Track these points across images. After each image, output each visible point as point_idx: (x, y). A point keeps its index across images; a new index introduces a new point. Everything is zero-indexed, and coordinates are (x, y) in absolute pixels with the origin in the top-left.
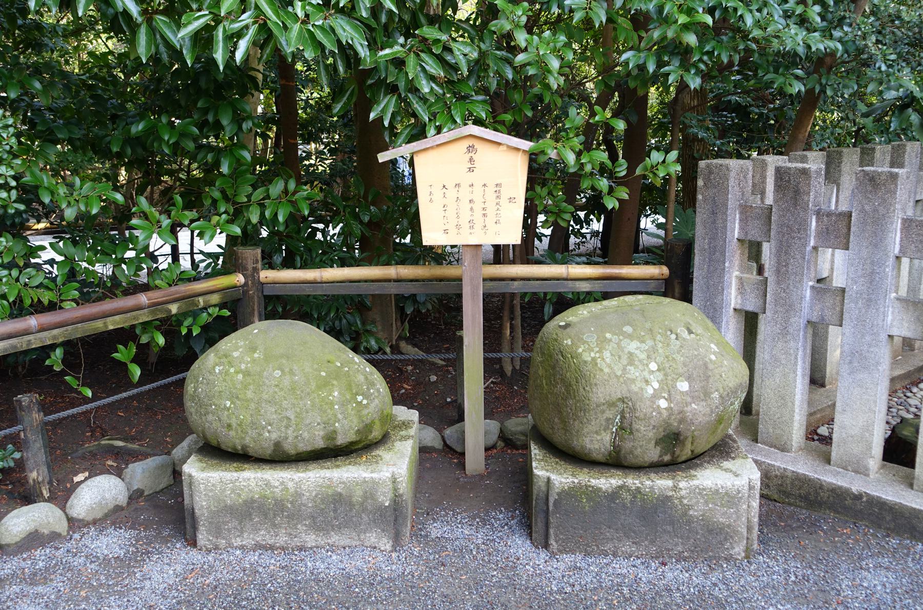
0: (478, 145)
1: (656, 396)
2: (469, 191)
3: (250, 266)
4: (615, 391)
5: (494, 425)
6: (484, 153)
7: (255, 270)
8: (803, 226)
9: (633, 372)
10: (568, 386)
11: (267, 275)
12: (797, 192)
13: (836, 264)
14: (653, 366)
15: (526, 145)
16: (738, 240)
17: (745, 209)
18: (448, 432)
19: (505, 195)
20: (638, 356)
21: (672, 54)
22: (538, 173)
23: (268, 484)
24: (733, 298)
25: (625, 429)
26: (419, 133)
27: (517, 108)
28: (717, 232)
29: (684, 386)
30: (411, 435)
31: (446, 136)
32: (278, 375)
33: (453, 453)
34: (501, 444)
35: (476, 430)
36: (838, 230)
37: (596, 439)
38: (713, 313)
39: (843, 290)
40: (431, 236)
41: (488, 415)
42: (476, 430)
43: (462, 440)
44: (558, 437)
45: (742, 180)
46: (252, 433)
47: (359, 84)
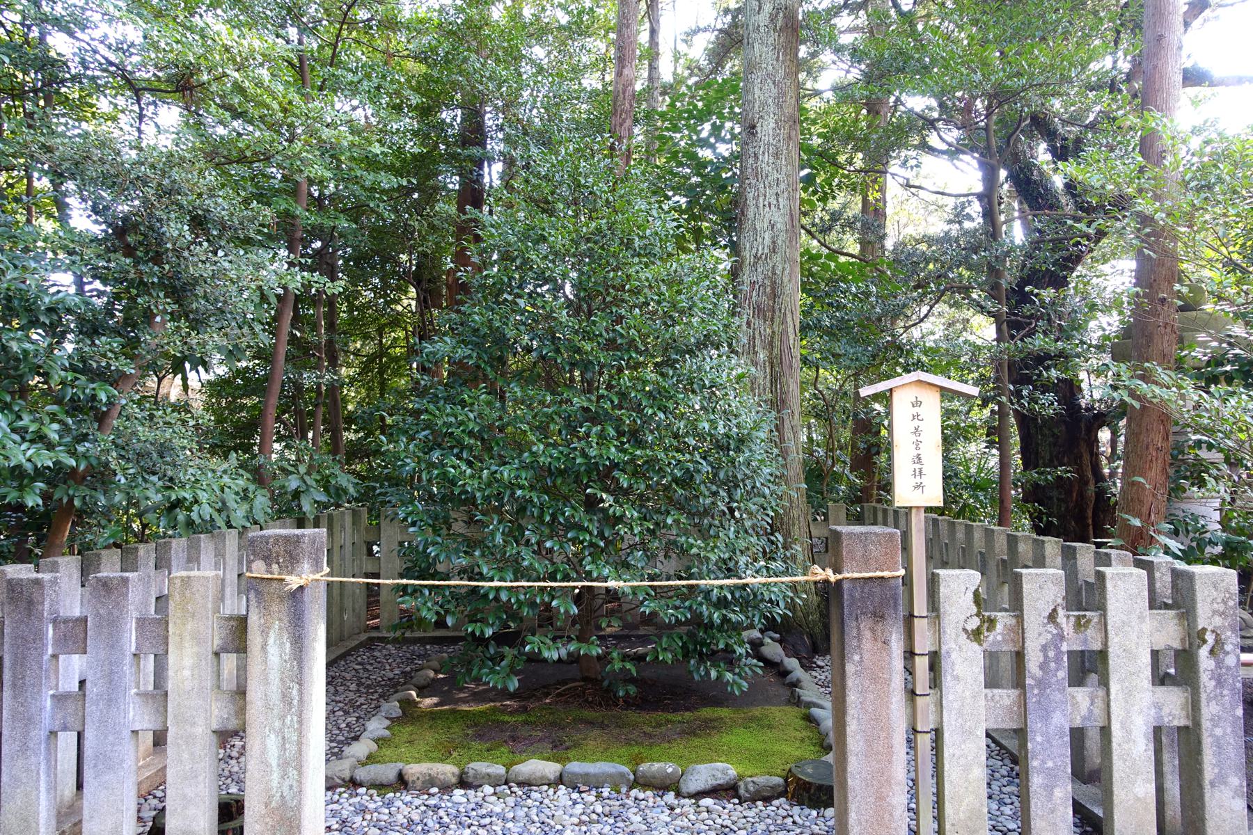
8: (39, 636)
12: (30, 603)
13: (73, 667)
36: (75, 635)
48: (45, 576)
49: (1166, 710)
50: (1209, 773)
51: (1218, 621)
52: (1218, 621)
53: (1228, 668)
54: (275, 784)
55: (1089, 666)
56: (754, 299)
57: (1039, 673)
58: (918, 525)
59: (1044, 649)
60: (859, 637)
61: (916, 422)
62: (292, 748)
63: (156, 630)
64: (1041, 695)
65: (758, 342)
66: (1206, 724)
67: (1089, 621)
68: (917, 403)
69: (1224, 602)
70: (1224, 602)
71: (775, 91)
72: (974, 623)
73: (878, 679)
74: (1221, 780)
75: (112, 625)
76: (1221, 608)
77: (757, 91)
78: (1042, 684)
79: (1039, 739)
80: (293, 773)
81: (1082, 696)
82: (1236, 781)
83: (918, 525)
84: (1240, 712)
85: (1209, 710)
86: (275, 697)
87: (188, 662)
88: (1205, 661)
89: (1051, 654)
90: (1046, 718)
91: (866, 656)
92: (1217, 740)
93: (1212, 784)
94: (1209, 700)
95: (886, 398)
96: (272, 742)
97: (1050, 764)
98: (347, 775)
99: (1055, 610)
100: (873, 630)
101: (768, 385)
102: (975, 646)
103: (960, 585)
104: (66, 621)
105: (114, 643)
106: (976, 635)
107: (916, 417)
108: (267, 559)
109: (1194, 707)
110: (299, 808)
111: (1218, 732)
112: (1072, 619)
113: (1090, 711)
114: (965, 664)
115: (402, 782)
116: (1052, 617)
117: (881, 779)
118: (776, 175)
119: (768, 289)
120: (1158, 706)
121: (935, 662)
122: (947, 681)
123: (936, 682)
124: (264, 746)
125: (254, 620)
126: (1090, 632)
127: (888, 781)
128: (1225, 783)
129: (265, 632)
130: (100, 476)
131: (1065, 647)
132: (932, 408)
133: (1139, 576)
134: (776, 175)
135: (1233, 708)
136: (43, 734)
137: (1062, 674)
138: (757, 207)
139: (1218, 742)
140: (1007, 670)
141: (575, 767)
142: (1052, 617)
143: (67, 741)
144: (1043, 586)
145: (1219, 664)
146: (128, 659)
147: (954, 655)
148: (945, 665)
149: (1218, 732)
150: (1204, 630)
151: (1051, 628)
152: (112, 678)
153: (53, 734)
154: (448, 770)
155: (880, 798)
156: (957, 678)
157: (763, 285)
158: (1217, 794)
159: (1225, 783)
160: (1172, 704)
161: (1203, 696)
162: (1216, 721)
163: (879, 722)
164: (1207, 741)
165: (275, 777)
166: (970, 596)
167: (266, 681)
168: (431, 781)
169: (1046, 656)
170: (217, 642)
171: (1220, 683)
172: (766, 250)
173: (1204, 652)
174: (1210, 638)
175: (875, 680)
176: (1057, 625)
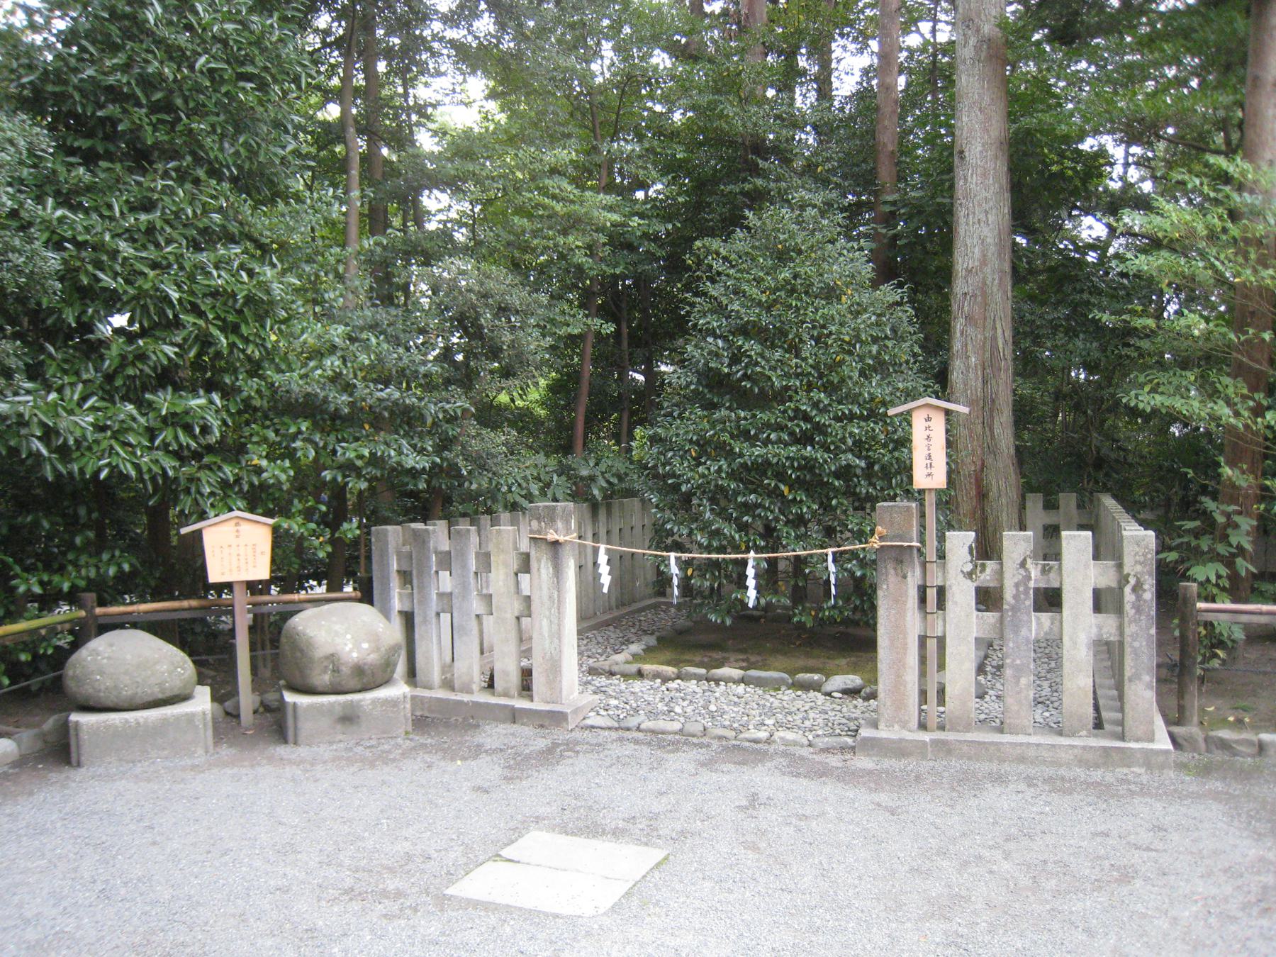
0: (242, 522)
1: (351, 651)
2: (236, 548)
3: (89, 604)
4: (330, 650)
5: (258, 699)
6: (245, 527)
7: (93, 608)
8: (429, 559)
9: (338, 640)
10: (302, 651)
11: (99, 611)
12: (424, 542)
13: (446, 581)
14: (349, 636)
15: (271, 521)
16: (398, 572)
17: (399, 554)
18: (227, 704)
19: (259, 551)
20: (337, 628)
21: (350, 470)
22: (279, 537)
23: (127, 721)
24: (397, 604)
25: (336, 671)
26: (202, 516)
27: (259, 499)
28: (385, 566)
29: (365, 646)
30: (202, 702)
31: (222, 517)
32: (130, 656)
33: (233, 715)
34: (261, 710)
35: (247, 699)
36: (446, 561)
37: (323, 678)
38: (386, 613)
39: (451, 594)
40: (214, 576)
41: (254, 690)
42: (247, 699)
43: (237, 707)
44: (298, 681)
45: (392, 539)
46: (115, 693)
47: (169, 489)
48: (431, 528)
49: (1105, 630)
50: (1128, 672)
51: (1139, 568)
52: (1139, 568)
53: (1145, 601)
54: (547, 646)
55: (1050, 600)
56: (966, 308)
57: (1012, 602)
58: (930, 500)
59: (1017, 585)
60: (887, 574)
61: (928, 432)
62: (555, 627)
63: (485, 560)
64: (1013, 616)
65: (970, 348)
66: (1128, 639)
67: (1051, 568)
68: (929, 419)
69: (1144, 555)
70: (1144, 555)
71: (981, 117)
72: (969, 567)
73: (899, 600)
74: (1137, 676)
75: (462, 554)
76: (1142, 559)
77: (965, 119)
78: (1014, 609)
79: (1011, 645)
80: (556, 641)
81: (1045, 617)
82: (1149, 678)
83: (930, 500)
84: (1153, 631)
85: (1130, 629)
86: (546, 598)
87: (502, 577)
88: (1129, 596)
89: (1021, 589)
90: (1016, 632)
91: (891, 586)
92: (1135, 652)
93: (1130, 681)
94: (1130, 622)
95: (907, 418)
96: (545, 623)
97: (1018, 662)
98: (607, 668)
99: (1025, 560)
100: (895, 569)
101: (980, 385)
102: (969, 582)
103: (961, 542)
104: (441, 553)
105: (464, 566)
106: (969, 575)
107: (928, 428)
108: (539, 519)
109: (1121, 629)
110: (560, 659)
111: (1136, 644)
112: (1040, 567)
113: (1051, 629)
114: (962, 594)
115: (640, 674)
116: (1023, 564)
117: (899, 664)
118: (985, 194)
119: (979, 299)
120: (1100, 628)
121: (941, 591)
122: (949, 605)
123: (941, 605)
124: (540, 626)
125: (533, 554)
126: (1052, 575)
127: (904, 665)
128: (1140, 679)
129: (539, 561)
130: (453, 471)
131: (1032, 584)
132: (939, 424)
133: (1086, 537)
134: (985, 194)
135: (1148, 629)
136: (433, 614)
137: (1029, 602)
138: (967, 224)
139: (1135, 652)
140: (987, 599)
141: (753, 673)
142: (1023, 564)
143: (445, 618)
144: (1017, 544)
145: (1139, 598)
146: (472, 575)
147: (954, 588)
148: (948, 595)
149: (1136, 644)
150: (1128, 575)
151: (1022, 572)
152: (465, 587)
153: (438, 614)
154: (670, 670)
155: (898, 676)
156: (956, 603)
157: (974, 296)
158: (1133, 687)
159: (1140, 679)
160: (1107, 625)
161: (1126, 620)
162: (1135, 637)
163: (899, 629)
164: (1128, 650)
165: (547, 642)
166: (966, 549)
167: (541, 588)
168: (656, 675)
169: (1017, 590)
170: (516, 567)
171: (1138, 610)
172: (977, 263)
173: (1128, 590)
174: (1132, 581)
175: (896, 601)
176: (1027, 570)
